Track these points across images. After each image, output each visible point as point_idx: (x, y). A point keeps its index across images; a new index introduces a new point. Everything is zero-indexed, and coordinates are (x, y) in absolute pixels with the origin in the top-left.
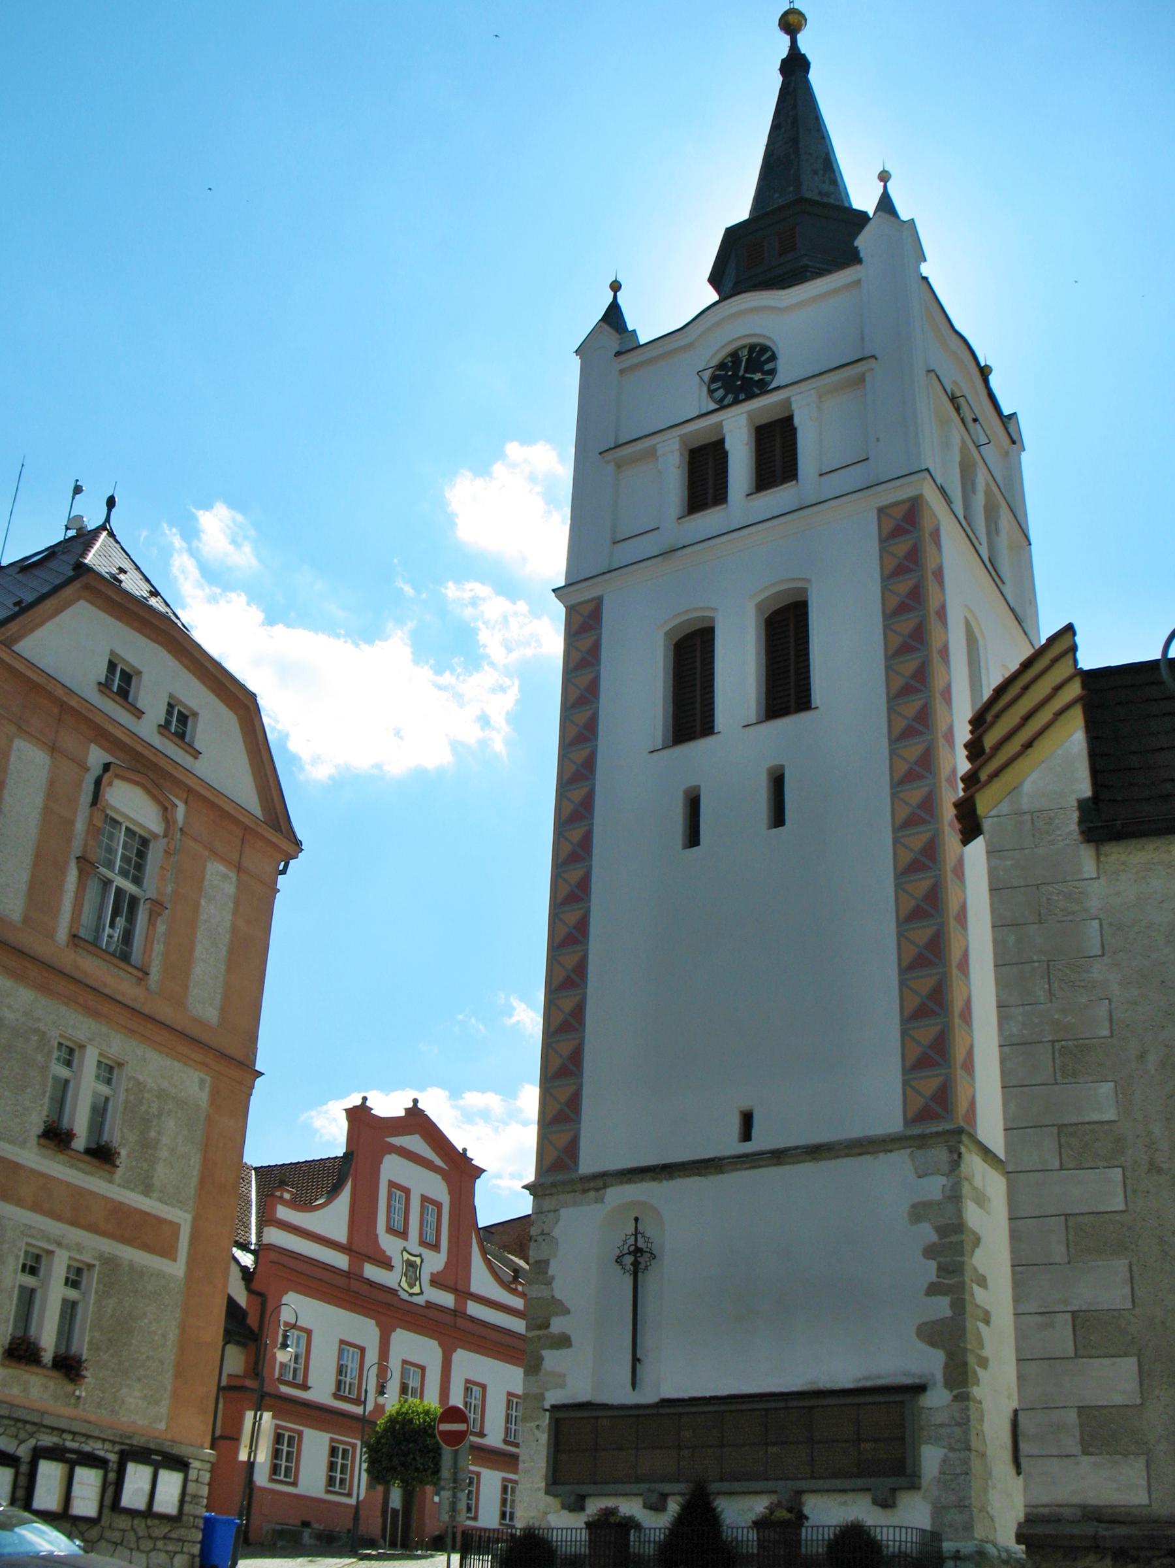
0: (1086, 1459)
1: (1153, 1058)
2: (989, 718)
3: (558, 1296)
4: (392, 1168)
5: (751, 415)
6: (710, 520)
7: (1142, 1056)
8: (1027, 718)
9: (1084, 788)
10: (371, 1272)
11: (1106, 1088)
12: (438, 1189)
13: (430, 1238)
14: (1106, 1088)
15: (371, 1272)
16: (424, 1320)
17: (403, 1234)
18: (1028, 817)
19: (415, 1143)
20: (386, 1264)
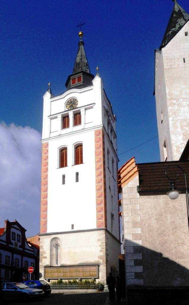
0: (135, 279)
1: (147, 225)
2: (121, 172)
3: (44, 251)
4: (13, 230)
5: (74, 112)
6: (66, 131)
7: (145, 224)
8: (129, 172)
9: (138, 185)
10: (10, 246)
11: (140, 229)
12: (20, 233)
13: (19, 240)
14: (140, 229)
15: (10, 246)
16: (18, 252)
17: (15, 240)
18: (129, 188)
19: (16, 226)
20: (12, 244)
